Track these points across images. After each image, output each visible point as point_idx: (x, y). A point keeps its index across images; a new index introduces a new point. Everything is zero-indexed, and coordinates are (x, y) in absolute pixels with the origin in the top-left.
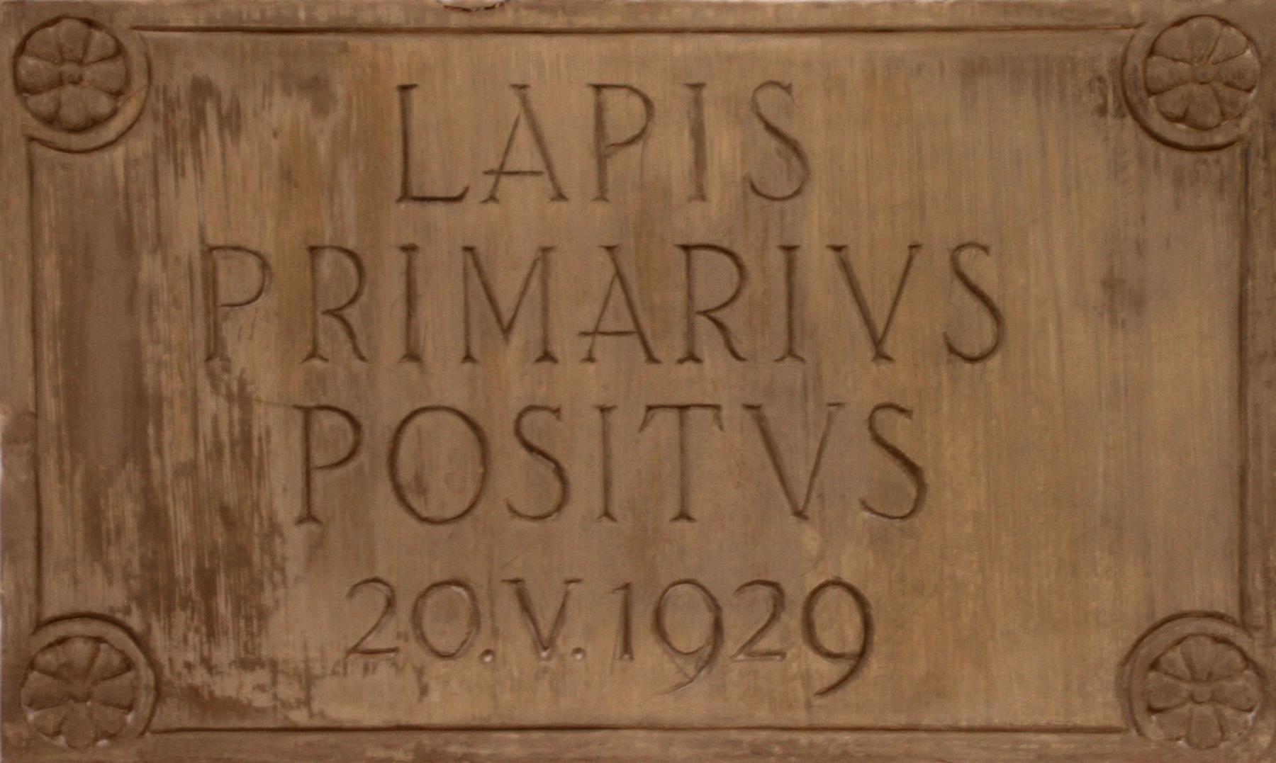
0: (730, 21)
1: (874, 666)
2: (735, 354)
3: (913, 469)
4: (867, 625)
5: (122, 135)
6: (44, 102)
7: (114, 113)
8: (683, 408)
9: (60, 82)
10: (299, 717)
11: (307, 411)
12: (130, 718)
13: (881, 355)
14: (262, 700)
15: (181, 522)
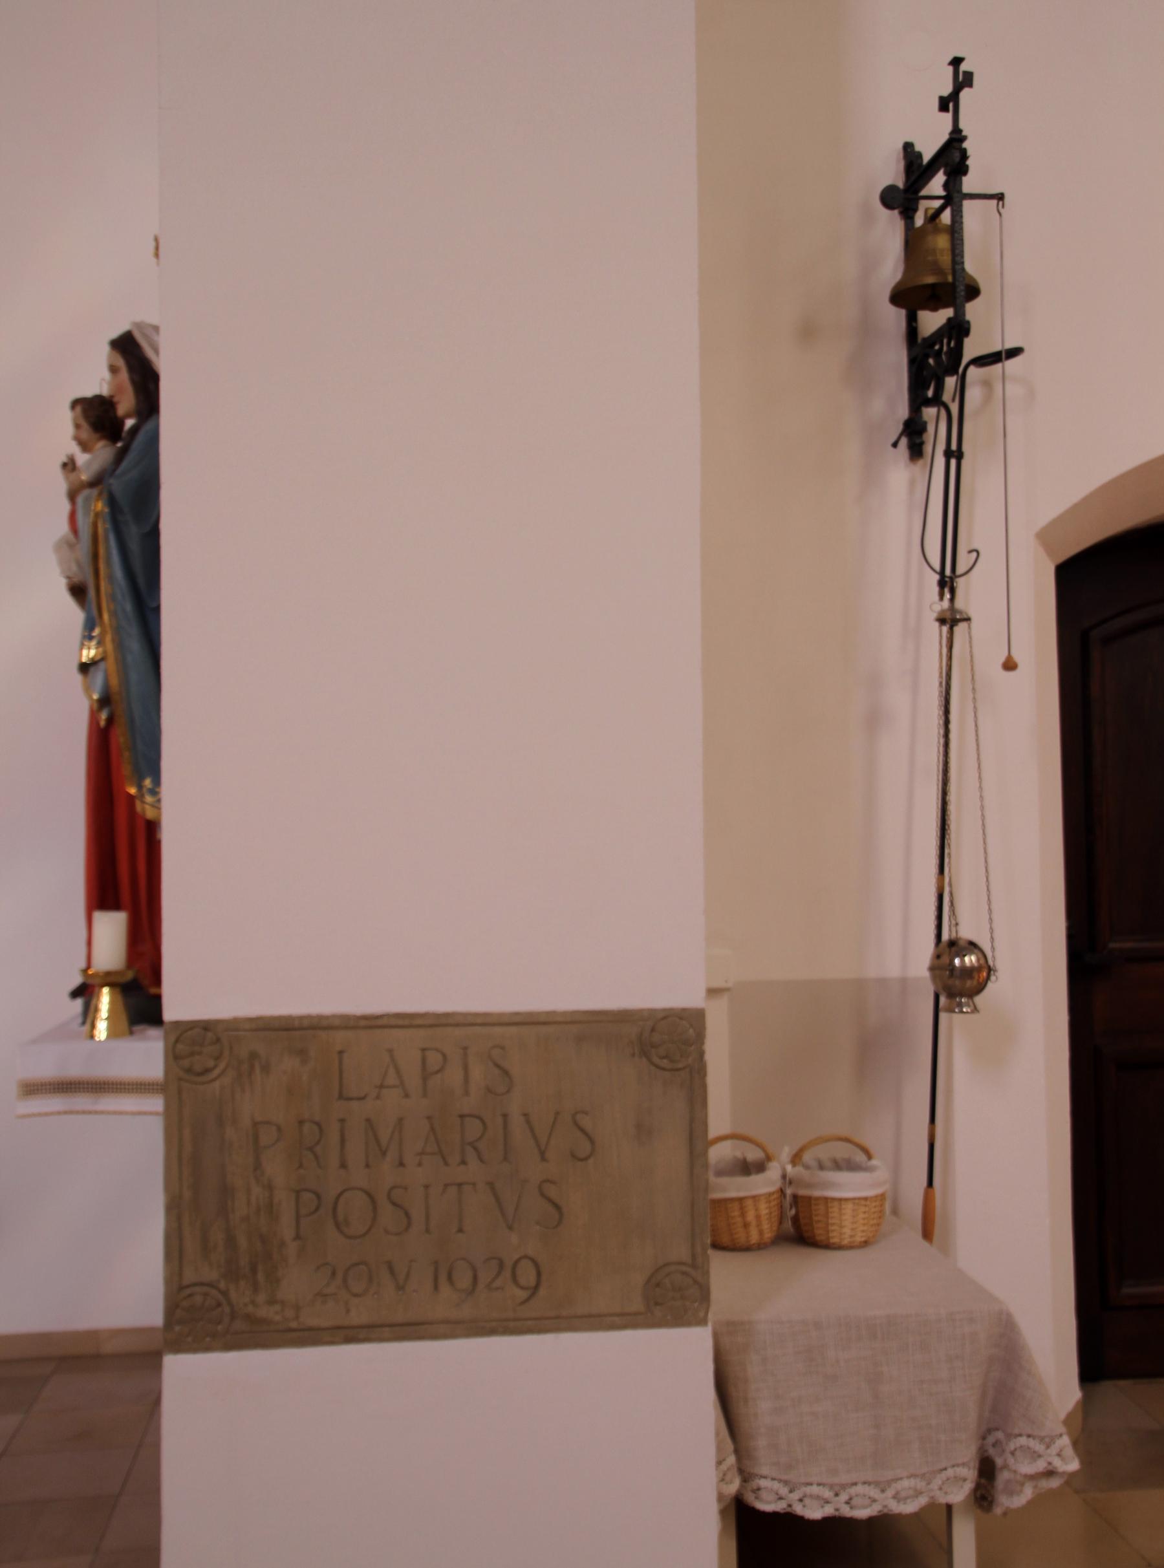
0: (479, 1021)
1: (542, 1292)
2: (482, 1161)
3: (558, 1207)
4: (539, 1274)
5: (219, 1076)
6: (186, 1063)
7: (215, 1067)
8: (460, 1185)
9: (192, 1054)
10: (294, 1325)
11: (298, 1192)
12: (220, 1327)
13: (543, 1159)
14: (278, 1318)
15: (243, 1242)
